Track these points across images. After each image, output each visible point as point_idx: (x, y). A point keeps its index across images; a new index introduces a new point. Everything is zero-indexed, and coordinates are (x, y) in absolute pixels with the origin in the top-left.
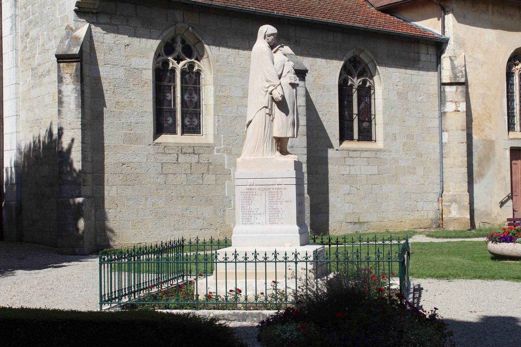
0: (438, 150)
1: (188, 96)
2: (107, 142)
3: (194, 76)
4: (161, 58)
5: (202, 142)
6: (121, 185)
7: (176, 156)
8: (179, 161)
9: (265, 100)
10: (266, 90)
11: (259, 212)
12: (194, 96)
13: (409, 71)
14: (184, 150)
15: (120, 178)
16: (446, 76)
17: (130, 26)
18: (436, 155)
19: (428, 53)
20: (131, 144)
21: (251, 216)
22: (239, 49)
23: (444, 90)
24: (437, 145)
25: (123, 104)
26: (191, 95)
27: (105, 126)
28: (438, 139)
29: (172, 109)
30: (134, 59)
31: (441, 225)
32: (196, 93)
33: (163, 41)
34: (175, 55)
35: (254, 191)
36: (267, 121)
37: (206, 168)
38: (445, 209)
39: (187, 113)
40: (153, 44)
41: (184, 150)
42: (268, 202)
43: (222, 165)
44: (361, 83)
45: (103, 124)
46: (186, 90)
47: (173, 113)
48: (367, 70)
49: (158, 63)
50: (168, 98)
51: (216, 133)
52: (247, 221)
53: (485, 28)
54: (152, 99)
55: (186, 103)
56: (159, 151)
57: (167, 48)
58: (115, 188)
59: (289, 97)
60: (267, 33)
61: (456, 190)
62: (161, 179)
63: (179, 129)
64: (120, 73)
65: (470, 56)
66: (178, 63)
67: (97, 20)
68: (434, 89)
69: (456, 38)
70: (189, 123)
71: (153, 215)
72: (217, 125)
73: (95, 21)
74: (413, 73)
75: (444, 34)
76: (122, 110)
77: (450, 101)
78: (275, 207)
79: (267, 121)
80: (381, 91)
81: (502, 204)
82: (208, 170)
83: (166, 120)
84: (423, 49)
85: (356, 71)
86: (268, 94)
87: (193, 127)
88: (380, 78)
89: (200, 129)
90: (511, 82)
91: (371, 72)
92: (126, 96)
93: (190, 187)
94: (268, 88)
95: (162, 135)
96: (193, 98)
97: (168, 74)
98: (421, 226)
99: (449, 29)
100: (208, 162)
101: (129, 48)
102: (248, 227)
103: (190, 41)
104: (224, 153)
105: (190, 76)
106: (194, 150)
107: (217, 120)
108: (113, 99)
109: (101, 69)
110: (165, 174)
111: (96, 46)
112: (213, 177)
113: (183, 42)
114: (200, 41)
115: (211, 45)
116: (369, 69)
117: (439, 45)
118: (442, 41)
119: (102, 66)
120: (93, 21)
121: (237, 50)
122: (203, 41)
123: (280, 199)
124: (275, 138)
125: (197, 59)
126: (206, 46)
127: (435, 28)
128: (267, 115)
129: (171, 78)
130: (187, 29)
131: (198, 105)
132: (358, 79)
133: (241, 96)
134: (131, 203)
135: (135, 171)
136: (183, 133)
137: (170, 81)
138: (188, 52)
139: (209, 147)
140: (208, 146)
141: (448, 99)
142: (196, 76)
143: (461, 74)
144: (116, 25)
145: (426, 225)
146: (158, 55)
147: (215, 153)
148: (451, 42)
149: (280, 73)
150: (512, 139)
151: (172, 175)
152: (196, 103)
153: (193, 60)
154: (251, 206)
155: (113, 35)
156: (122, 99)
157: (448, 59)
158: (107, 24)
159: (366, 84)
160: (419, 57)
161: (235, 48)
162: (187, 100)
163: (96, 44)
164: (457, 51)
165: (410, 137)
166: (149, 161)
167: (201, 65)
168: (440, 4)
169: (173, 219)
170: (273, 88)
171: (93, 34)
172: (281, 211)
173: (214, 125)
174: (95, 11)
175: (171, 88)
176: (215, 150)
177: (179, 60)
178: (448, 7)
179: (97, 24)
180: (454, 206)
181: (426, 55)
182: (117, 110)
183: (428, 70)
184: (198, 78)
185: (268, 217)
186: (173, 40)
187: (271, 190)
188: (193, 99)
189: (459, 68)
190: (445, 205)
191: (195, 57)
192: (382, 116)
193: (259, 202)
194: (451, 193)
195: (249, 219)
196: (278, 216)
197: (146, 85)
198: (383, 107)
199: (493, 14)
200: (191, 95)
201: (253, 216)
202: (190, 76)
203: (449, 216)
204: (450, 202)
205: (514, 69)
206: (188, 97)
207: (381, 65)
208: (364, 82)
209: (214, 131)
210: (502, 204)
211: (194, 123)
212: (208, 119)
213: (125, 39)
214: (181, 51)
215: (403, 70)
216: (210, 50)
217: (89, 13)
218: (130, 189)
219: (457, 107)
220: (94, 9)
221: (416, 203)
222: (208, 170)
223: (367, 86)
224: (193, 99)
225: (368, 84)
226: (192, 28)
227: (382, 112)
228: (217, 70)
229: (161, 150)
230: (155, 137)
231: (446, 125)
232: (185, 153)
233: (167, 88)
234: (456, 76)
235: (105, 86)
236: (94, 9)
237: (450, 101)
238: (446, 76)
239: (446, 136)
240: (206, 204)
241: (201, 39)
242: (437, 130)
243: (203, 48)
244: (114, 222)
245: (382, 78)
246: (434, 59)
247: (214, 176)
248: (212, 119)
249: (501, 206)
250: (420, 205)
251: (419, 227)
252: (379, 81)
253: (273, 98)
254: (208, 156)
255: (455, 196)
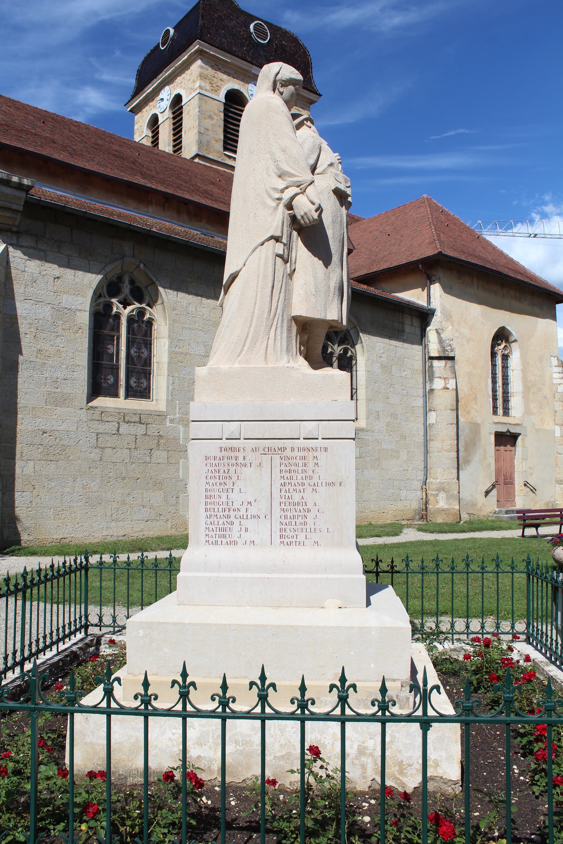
0: (422, 433)
1: (136, 350)
2: (22, 401)
3: (144, 326)
4: (102, 300)
5: (151, 408)
6: (40, 460)
7: (117, 425)
8: (120, 432)
9: (276, 222)
10: (277, 195)
11: (253, 511)
12: (143, 351)
13: (393, 342)
14: (127, 418)
15: (40, 450)
16: (434, 349)
17: (62, 253)
18: (420, 438)
19: (412, 325)
20: (56, 406)
21: (232, 523)
22: (202, 296)
23: (432, 365)
24: (421, 427)
25: (47, 353)
26: (139, 349)
27: (20, 380)
28: (422, 420)
29: (114, 365)
30: (65, 297)
31: (425, 517)
32: (146, 347)
33: (105, 277)
34: (122, 297)
35: (240, 455)
36: (279, 275)
37: (156, 441)
38: (431, 498)
39: (133, 372)
40: (92, 280)
41: (127, 418)
42: (277, 482)
43: (176, 439)
44: (342, 352)
45: (16, 378)
46: (133, 342)
47: (115, 371)
48: (349, 337)
49: (98, 305)
50: (109, 351)
51: (170, 398)
52: (221, 536)
53: (471, 302)
54: (87, 350)
55: (132, 359)
56: (94, 418)
57: (110, 289)
58: (31, 464)
59: (333, 222)
60: (279, 77)
61: (445, 477)
62: (95, 455)
63: (122, 391)
64: (46, 312)
65: (457, 330)
66: (125, 308)
67: (18, 241)
68: (418, 364)
69: (443, 309)
70: (135, 385)
71: (84, 501)
72: (171, 388)
73: (15, 242)
74: (397, 345)
75: (430, 305)
76: (45, 361)
77: (438, 377)
78: (296, 497)
79: (279, 275)
80: (364, 362)
81: (487, 493)
82: (158, 445)
83: (105, 379)
84: (407, 320)
85: (337, 338)
86: (281, 207)
87: (140, 390)
88: (363, 347)
89: (149, 393)
90: (494, 363)
91: (353, 340)
92: (52, 343)
93: (133, 465)
94: (282, 191)
95: (99, 398)
96: (142, 353)
97: (111, 320)
98: (404, 518)
99: (435, 299)
100: (158, 434)
101: (59, 282)
102: (222, 553)
103: (141, 282)
104: (179, 424)
105: (139, 326)
106: (141, 419)
107: (171, 382)
108: (34, 345)
109: (18, 305)
110: (101, 448)
111: (13, 275)
112: (164, 454)
113: (132, 282)
114: (154, 283)
115: (168, 288)
116: (351, 336)
117: (424, 316)
118: (429, 312)
119: (21, 301)
120: (12, 242)
121: (199, 298)
122: (157, 283)
123: (311, 478)
124: (296, 319)
125: (149, 305)
126: (161, 289)
127: (418, 298)
128: (279, 260)
129: (114, 326)
130: (138, 266)
131: (148, 362)
132: (339, 346)
133: (203, 354)
134: (53, 484)
135: (61, 443)
136: (127, 396)
137: (113, 330)
138: (138, 295)
139: (161, 416)
140: (158, 414)
141: (437, 374)
142: (147, 326)
143: (450, 348)
144: (43, 251)
145: (409, 516)
146: (97, 295)
147: (168, 424)
148: (438, 313)
149: (312, 161)
150: (496, 423)
151: (110, 449)
152: (146, 360)
153: (144, 305)
154: (231, 495)
155: (38, 262)
156: (46, 346)
157: (435, 332)
158: (31, 248)
159: (347, 353)
160: (403, 328)
161: (197, 295)
162: (134, 356)
163: (14, 272)
164: (444, 323)
165: (394, 416)
166: (80, 429)
167: (153, 313)
168: (425, 272)
169: (110, 507)
170: (297, 190)
171: (11, 259)
172: (314, 510)
173: (168, 388)
174: (15, 229)
175: (114, 338)
176: (168, 419)
177: (125, 304)
178: (433, 276)
179: (17, 246)
180: (442, 495)
181: (411, 326)
182: (38, 360)
183: (412, 343)
184: (149, 329)
185: (277, 527)
186: (120, 279)
187: (288, 453)
188: (142, 355)
189: (448, 342)
190: (431, 494)
191: (147, 301)
192: (365, 391)
193: (255, 485)
194: (438, 480)
195: (224, 530)
196: (305, 524)
197: (81, 331)
198: (367, 381)
199: (478, 288)
200: (139, 349)
201: (237, 522)
202: (139, 326)
203: (436, 507)
204: (437, 490)
205: (496, 349)
206: (136, 352)
207: (364, 332)
208: (346, 351)
209: (168, 396)
210: (487, 493)
211: (142, 385)
212: (160, 382)
213: (53, 269)
214: (128, 293)
215: (387, 341)
216: (167, 295)
217: (7, 231)
218: (53, 465)
219: (446, 384)
220: (14, 226)
221: (399, 491)
222: (158, 445)
223: (348, 355)
224: (142, 355)
225: (350, 354)
226: (145, 265)
227: (364, 386)
228: (174, 321)
229: (96, 416)
230: (89, 400)
231: (433, 403)
232: (128, 422)
233: (109, 338)
234: (444, 350)
235: (23, 327)
236: (14, 226)
237: (438, 377)
238: (434, 349)
239: (432, 418)
240: (154, 488)
241: (154, 280)
242: (421, 411)
243: (157, 291)
244: (29, 509)
245: (365, 347)
246: (418, 331)
247: (166, 452)
248: (165, 380)
249: (486, 496)
250: (403, 493)
251: (402, 519)
252: (361, 350)
253: (293, 218)
254: (158, 427)
255: (443, 483)
